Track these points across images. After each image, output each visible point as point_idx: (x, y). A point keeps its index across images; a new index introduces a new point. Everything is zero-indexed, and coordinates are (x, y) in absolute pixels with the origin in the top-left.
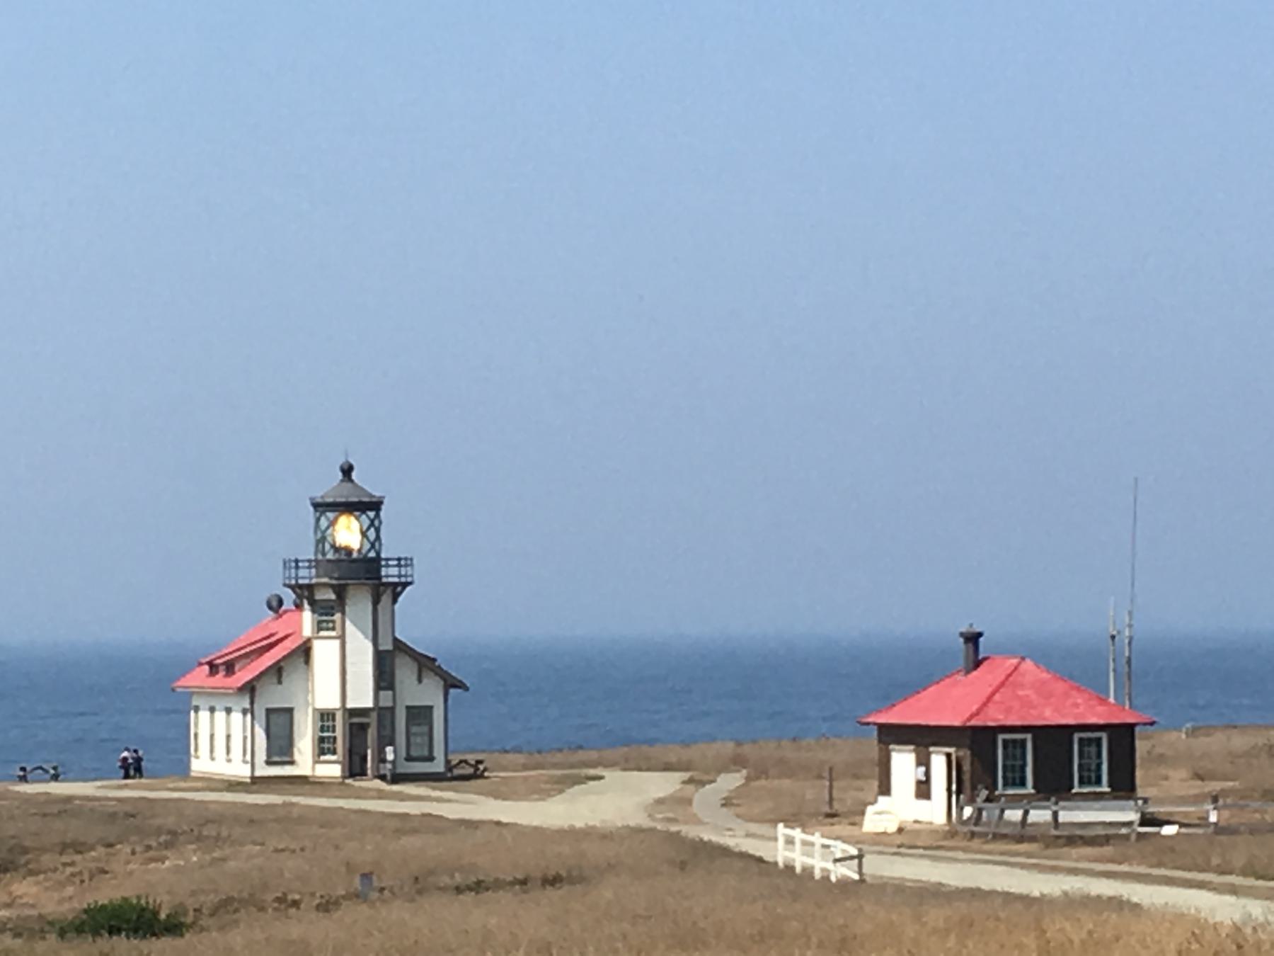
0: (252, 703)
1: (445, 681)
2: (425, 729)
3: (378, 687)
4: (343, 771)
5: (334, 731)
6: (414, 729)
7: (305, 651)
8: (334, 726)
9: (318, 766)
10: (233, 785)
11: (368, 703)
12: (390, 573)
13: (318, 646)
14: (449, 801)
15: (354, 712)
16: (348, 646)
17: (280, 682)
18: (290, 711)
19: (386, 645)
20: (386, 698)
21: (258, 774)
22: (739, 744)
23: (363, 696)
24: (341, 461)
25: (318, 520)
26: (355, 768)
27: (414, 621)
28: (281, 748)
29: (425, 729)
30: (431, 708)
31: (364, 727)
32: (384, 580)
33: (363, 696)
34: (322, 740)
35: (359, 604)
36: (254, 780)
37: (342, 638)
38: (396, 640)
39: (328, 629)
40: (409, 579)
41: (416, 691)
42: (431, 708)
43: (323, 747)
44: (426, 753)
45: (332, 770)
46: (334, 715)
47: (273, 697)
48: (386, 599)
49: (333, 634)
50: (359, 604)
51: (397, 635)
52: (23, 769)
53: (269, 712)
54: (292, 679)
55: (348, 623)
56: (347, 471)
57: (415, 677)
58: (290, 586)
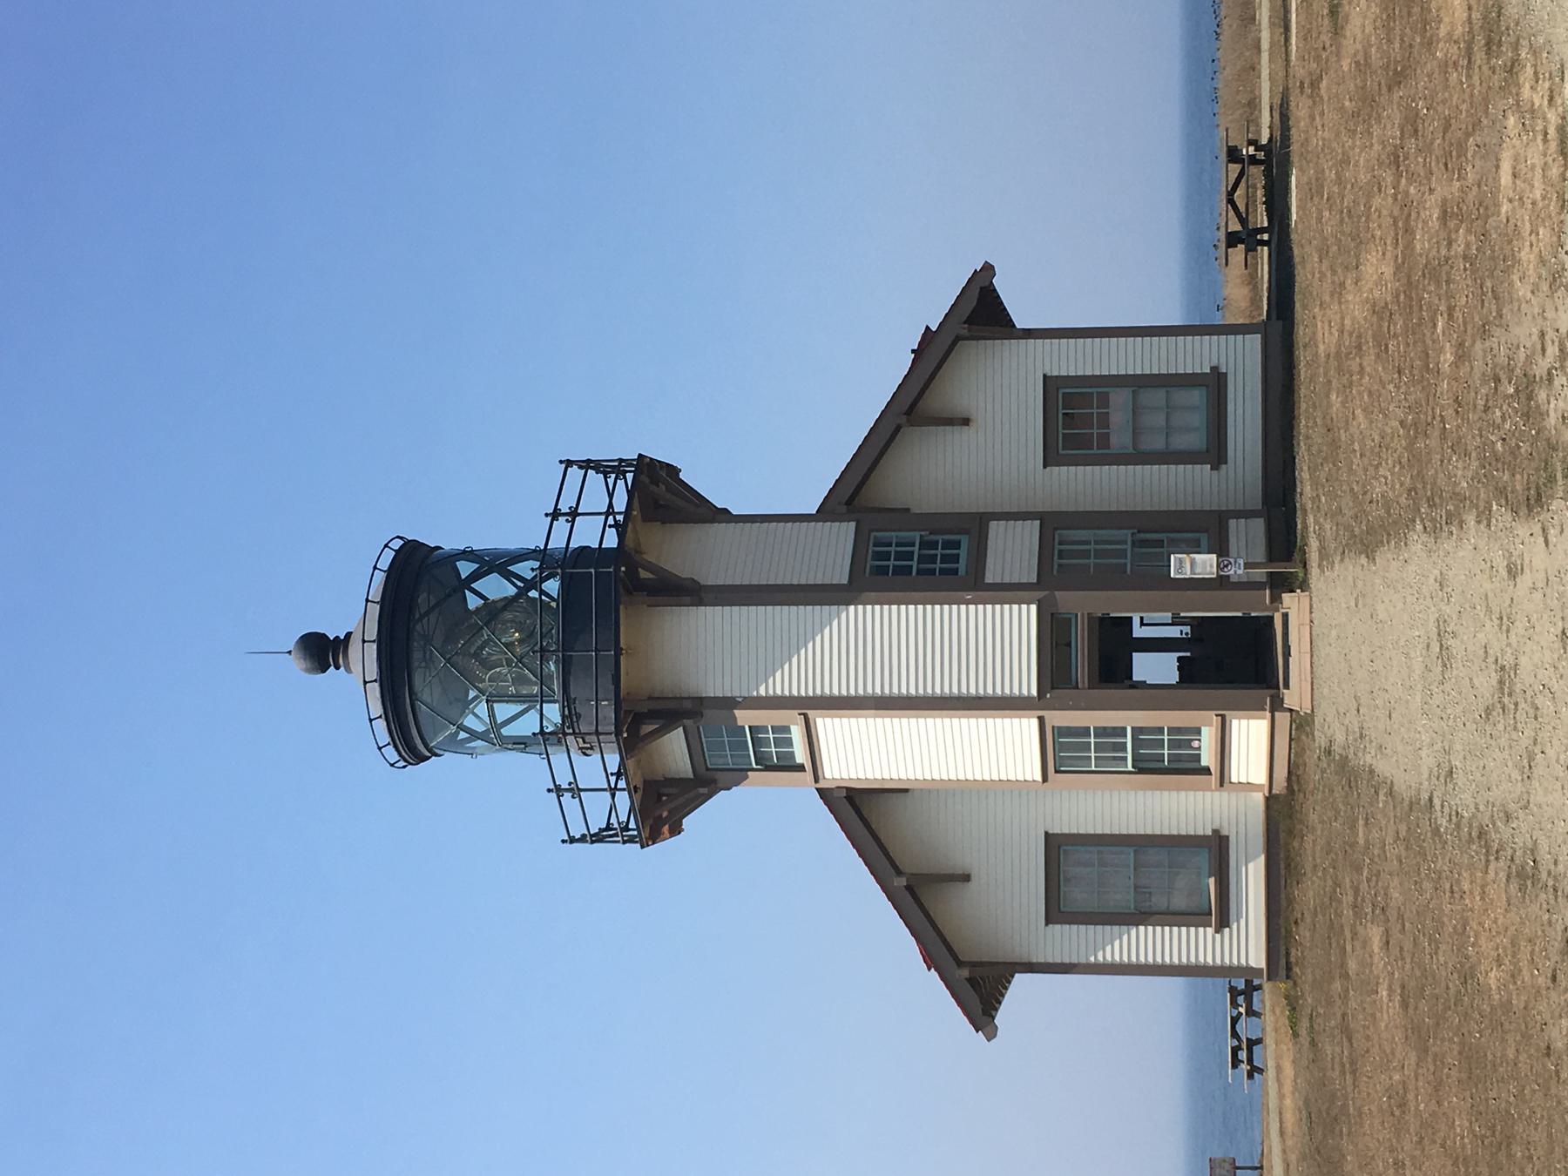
1: (958, 339)
4: (1254, 707)
5: (1121, 732)
6: (1120, 439)
7: (859, 810)
8: (1102, 732)
9: (1237, 774)
10: (1288, 954)
11: (1023, 619)
14: (1287, 40)
16: (835, 687)
17: (966, 878)
18: (1056, 846)
19: (834, 550)
20: (1013, 550)
22: (1434, 1142)
24: (295, 666)
26: (1236, 660)
27: (773, 456)
33: (1000, 638)
34: (1145, 766)
35: (703, 649)
36: (1288, 977)
38: (827, 511)
39: (789, 742)
41: (995, 448)
44: (1197, 397)
45: (1250, 744)
46: (1061, 732)
47: (1006, 902)
48: (683, 551)
49: (797, 734)
50: (703, 649)
53: (1056, 912)
54: (959, 842)
55: (780, 684)
56: (321, 651)
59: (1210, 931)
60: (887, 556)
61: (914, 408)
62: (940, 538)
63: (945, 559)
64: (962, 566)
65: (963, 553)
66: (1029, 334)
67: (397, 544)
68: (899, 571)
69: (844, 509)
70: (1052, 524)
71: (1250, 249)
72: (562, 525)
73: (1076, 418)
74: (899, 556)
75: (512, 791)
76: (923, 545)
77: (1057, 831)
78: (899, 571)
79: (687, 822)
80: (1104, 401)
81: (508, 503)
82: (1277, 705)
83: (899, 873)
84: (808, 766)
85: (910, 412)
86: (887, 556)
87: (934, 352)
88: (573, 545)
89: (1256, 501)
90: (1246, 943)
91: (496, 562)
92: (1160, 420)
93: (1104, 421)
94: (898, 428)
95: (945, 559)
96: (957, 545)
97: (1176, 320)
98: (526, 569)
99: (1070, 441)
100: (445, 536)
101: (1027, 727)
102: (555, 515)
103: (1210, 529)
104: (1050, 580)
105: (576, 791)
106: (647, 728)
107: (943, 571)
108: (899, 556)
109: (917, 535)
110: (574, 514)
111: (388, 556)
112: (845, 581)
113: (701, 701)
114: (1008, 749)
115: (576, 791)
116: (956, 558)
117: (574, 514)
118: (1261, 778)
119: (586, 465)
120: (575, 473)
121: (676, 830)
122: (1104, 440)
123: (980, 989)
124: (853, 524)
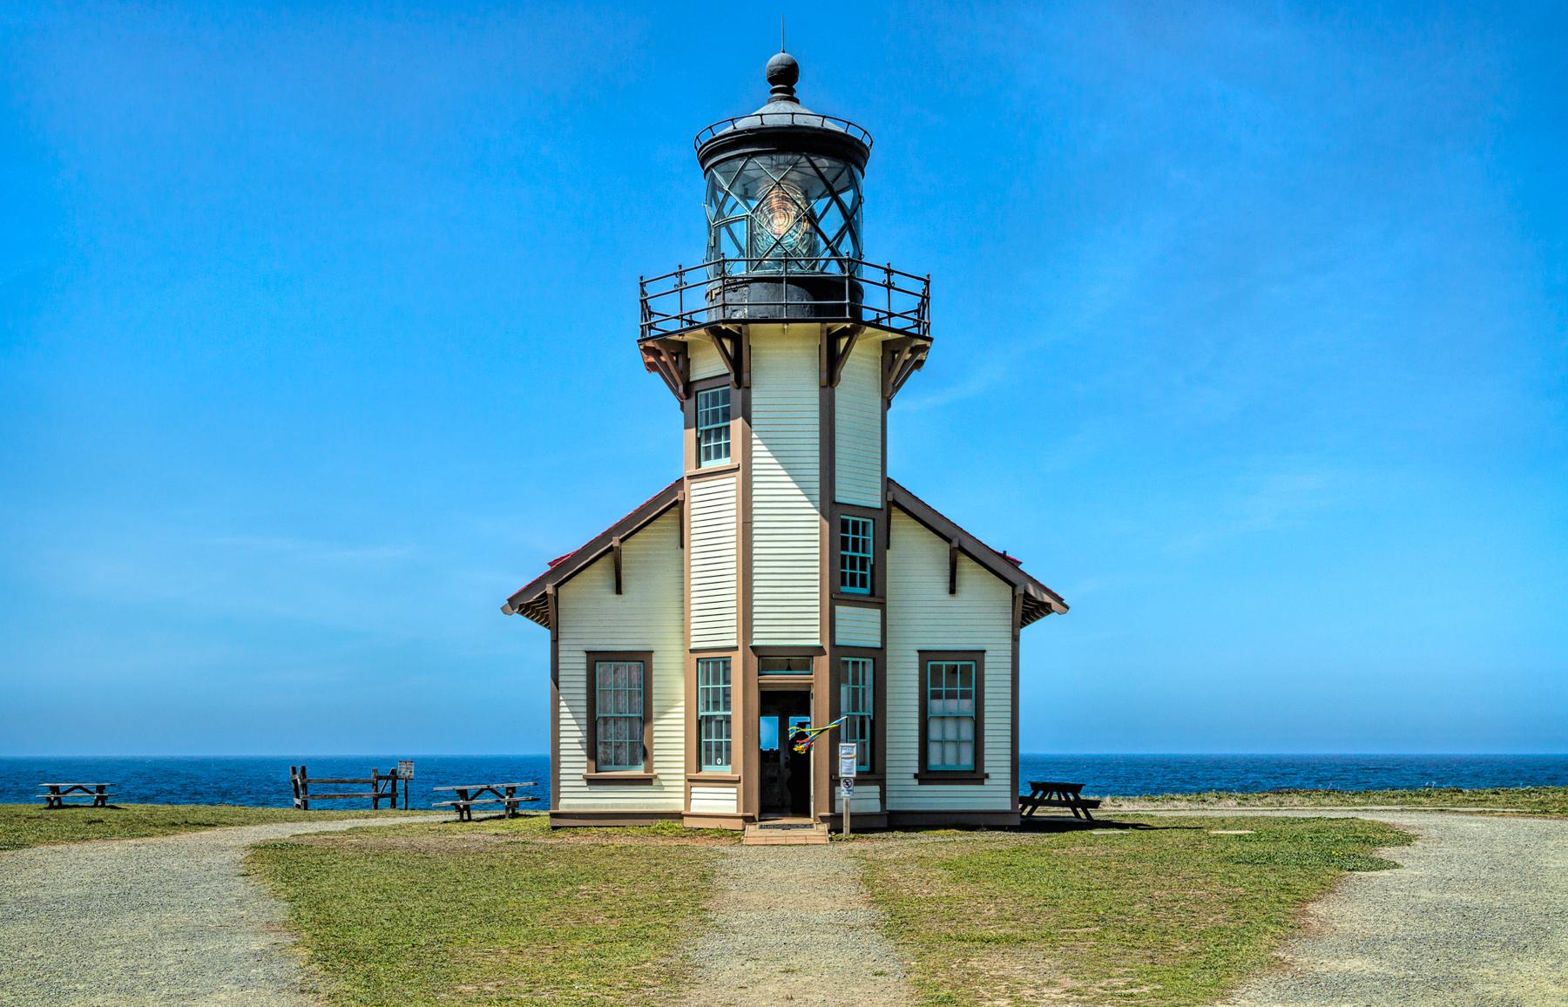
0: (555, 641)
1: (1014, 586)
2: (967, 706)
3: (837, 596)
5: (727, 706)
6: (936, 706)
7: (668, 507)
11: (812, 637)
12: (874, 299)
13: (695, 493)
15: (767, 658)
17: (619, 591)
18: (643, 659)
20: (859, 626)
23: (795, 612)
26: (782, 788)
27: (925, 443)
29: (967, 706)
31: (797, 702)
33: (795, 612)
37: (746, 471)
38: (888, 483)
41: (930, 611)
43: (707, 742)
44: (967, 761)
45: (720, 802)
46: (726, 663)
47: (598, 619)
48: (862, 359)
51: (546, 633)
52: (54, 789)
55: (759, 448)
57: (940, 582)
59: (584, 771)
60: (855, 531)
61: (961, 551)
62: (868, 572)
63: (853, 576)
64: (847, 589)
65: (858, 590)
66: (1015, 638)
67: (867, 142)
68: (844, 541)
69: (890, 498)
70: (878, 656)
71: (918, 311)
72: (880, 277)
74: (855, 541)
75: (697, 241)
76: (863, 560)
78: (844, 541)
79: (656, 375)
80: (965, 695)
81: (894, 239)
82: (748, 820)
83: (622, 541)
84: (700, 471)
85: (962, 549)
86: (855, 531)
87: (1002, 567)
88: (864, 285)
89: (892, 805)
90: (575, 796)
91: (851, 225)
92: (951, 734)
93: (951, 695)
94: (949, 541)
95: (853, 576)
96: (863, 585)
97: (1023, 751)
98: (846, 248)
99: (937, 671)
100: (872, 179)
102: (889, 272)
103: (873, 771)
104: (844, 658)
105: (680, 289)
106: (727, 343)
107: (844, 574)
108: (855, 541)
109: (871, 556)
110: (889, 286)
111: (858, 135)
112: (838, 499)
114: (714, 625)
115: (680, 289)
116: (853, 584)
117: (889, 286)
118: (693, 810)
119: (925, 298)
120: (918, 287)
121: (651, 367)
122: (937, 696)
123: (538, 604)
124: (879, 505)
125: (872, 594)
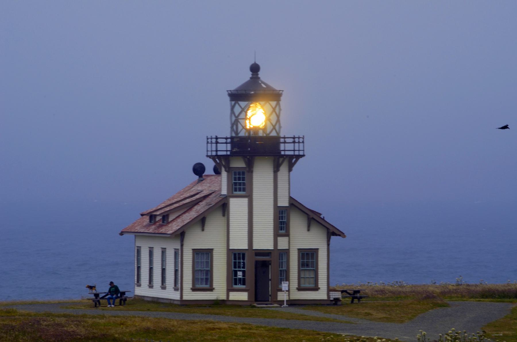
1: (328, 229)
3: (276, 235)
7: (223, 207)
12: (287, 148)
17: (203, 230)
19: (284, 202)
20: (283, 243)
21: (185, 298)
25: (233, 108)
27: (303, 183)
28: (203, 278)
30: (317, 250)
32: (283, 153)
33: (264, 241)
39: (240, 190)
40: (301, 153)
42: (317, 250)
43: (233, 282)
47: (197, 240)
48: (284, 169)
53: (196, 252)
56: (255, 69)
58: (210, 157)
70: (286, 252)
73: (308, 257)
77: (214, 251)
99: (303, 254)
101: (246, 247)
113: (252, 172)
114: (240, 243)
117: (294, 142)
125: (286, 232)
